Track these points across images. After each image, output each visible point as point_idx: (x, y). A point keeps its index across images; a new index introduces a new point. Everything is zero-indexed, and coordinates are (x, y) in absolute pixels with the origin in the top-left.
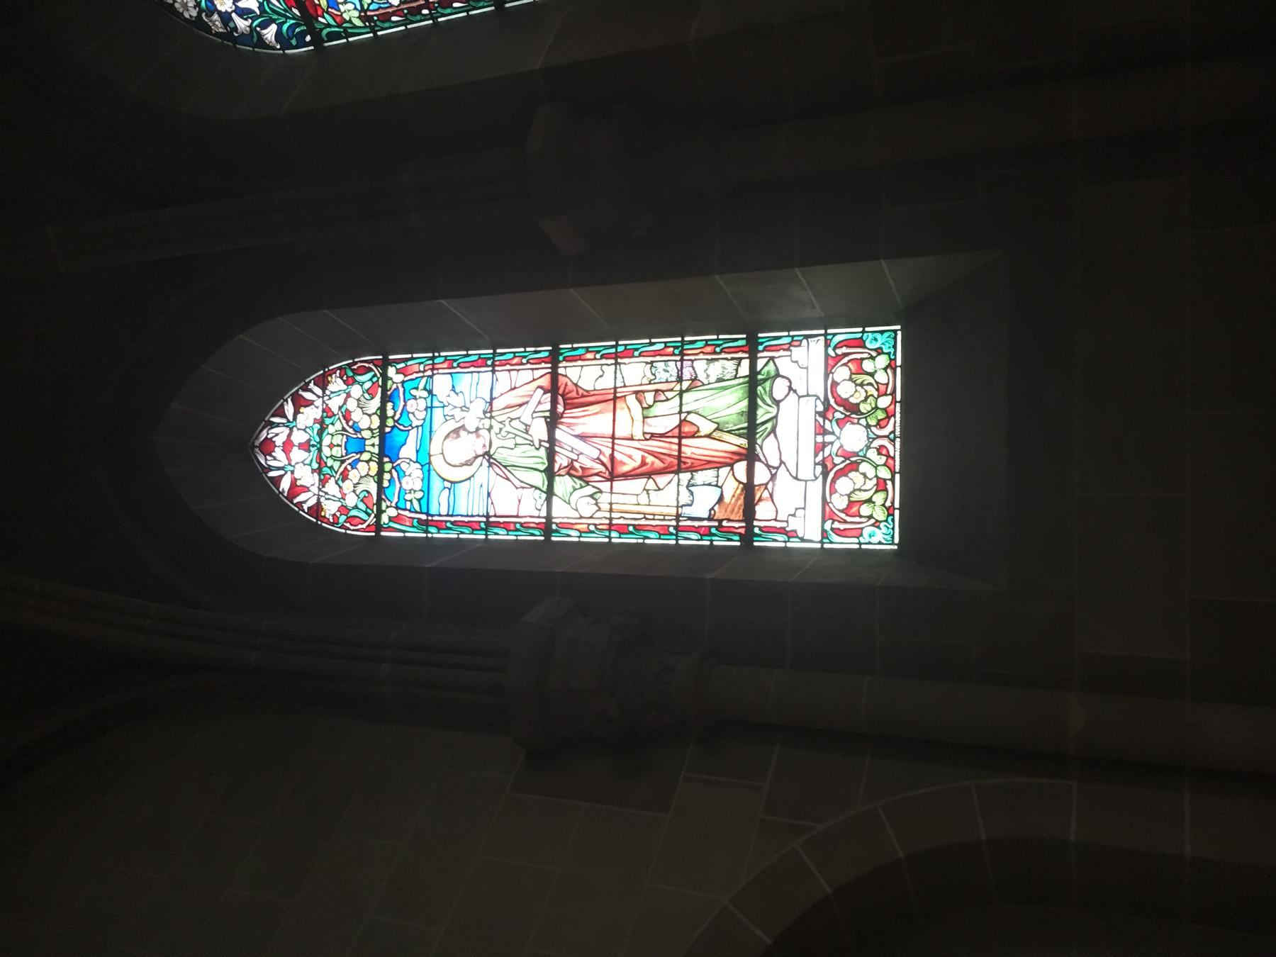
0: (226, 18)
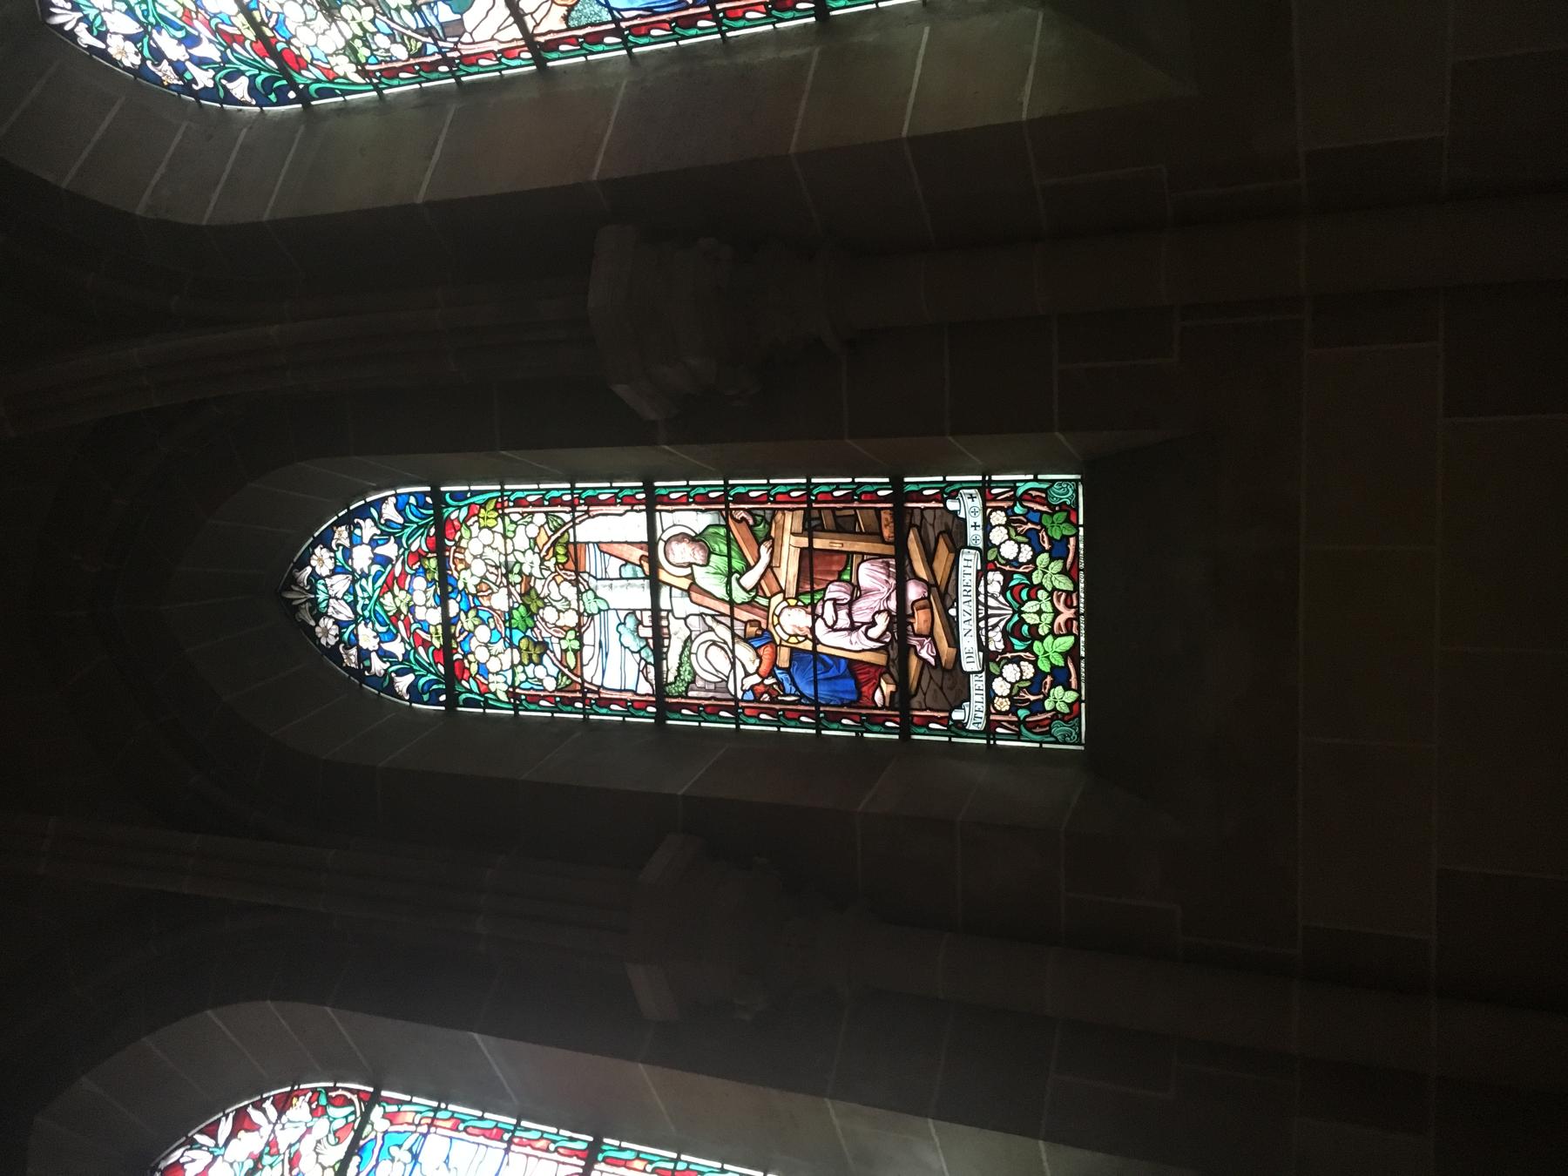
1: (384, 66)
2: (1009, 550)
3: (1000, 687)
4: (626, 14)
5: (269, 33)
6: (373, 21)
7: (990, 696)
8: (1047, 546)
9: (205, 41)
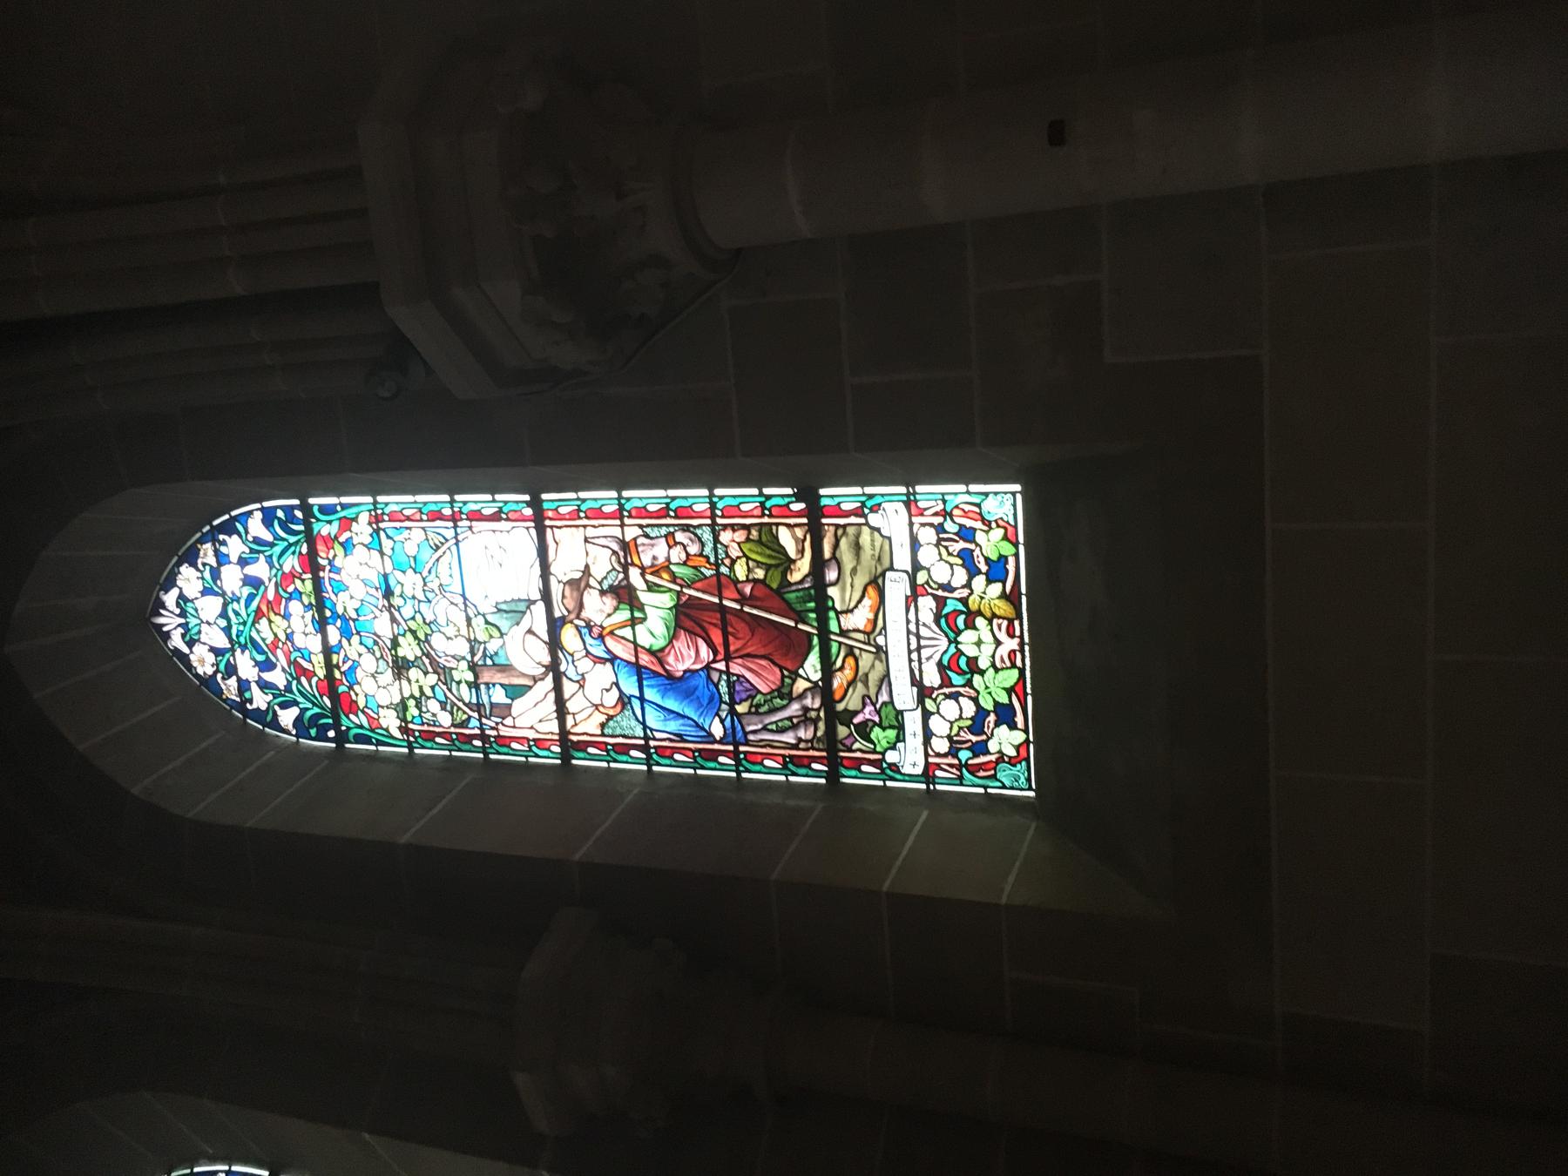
0: (243, 686)
1: (425, 728)
2: (941, 574)
3: (936, 724)
4: (658, 735)
5: (337, 675)
6: (433, 688)
7: (928, 735)
8: (984, 568)
9: (279, 668)
